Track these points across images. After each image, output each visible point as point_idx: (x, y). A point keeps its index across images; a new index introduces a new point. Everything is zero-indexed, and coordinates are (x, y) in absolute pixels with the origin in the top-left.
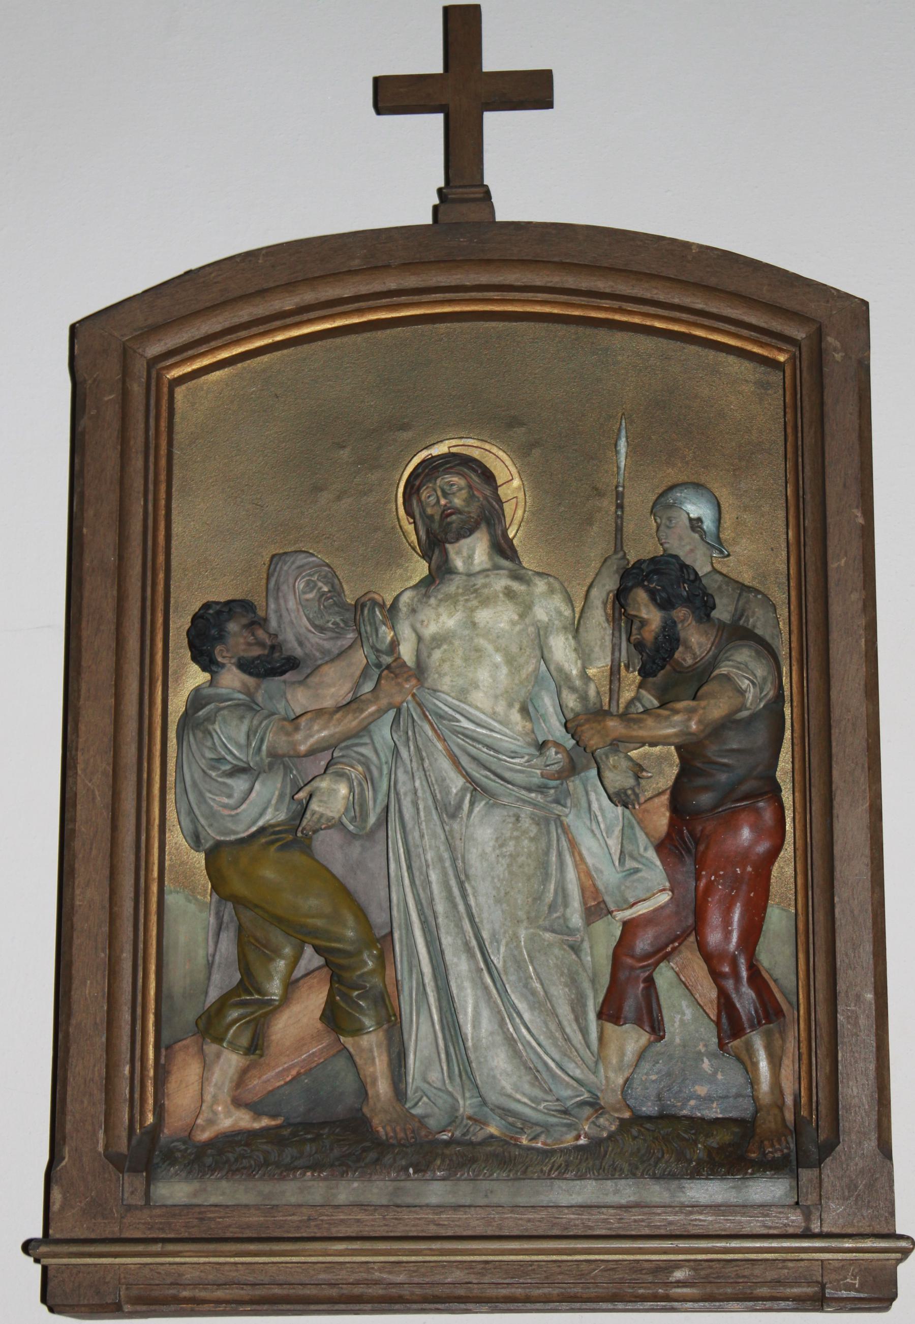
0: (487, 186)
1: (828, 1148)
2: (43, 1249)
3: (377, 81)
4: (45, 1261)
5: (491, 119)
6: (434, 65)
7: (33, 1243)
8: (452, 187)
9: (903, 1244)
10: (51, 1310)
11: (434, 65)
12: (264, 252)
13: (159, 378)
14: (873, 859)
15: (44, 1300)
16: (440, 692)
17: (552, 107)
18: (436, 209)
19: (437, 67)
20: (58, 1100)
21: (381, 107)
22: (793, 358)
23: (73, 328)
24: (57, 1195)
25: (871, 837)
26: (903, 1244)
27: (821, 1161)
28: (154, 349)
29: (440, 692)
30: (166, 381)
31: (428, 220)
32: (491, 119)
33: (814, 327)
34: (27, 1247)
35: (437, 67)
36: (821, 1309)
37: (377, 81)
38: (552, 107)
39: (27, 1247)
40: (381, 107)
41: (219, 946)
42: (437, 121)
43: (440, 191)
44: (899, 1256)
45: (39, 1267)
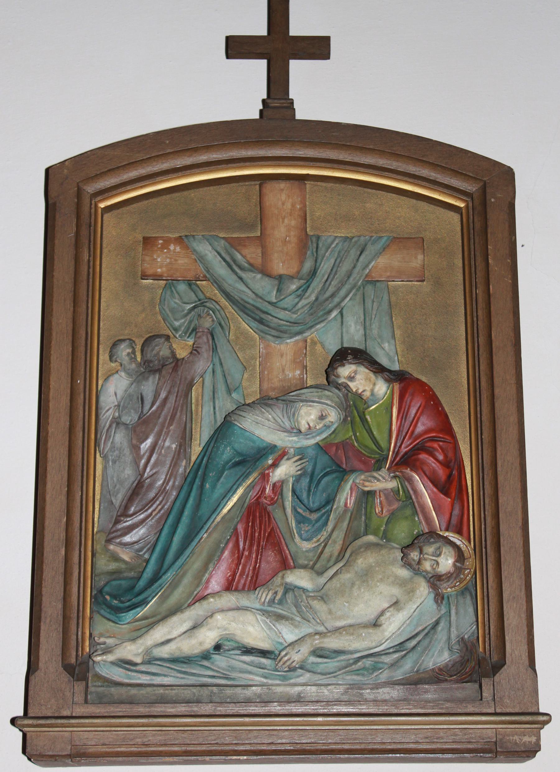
0: (292, 102)
1: (497, 667)
2: (26, 722)
3: (228, 38)
4: (25, 729)
9: (541, 718)
10: (29, 759)
12: (469, 154)
13: (96, 206)
15: (24, 752)
18: (261, 111)
19: (264, 32)
21: (326, 41)
22: (467, 207)
23: (47, 171)
25: (518, 411)
26: (541, 718)
27: (494, 675)
28: (91, 188)
30: (100, 211)
31: (257, 116)
33: (482, 184)
34: (13, 721)
35: (264, 32)
36: (493, 760)
37: (228, 38)
39: (13, 721)
40: (326, 41)
41: (366, 304)
43: (264, 101)
44: (539, 726)
45: (21, 734)
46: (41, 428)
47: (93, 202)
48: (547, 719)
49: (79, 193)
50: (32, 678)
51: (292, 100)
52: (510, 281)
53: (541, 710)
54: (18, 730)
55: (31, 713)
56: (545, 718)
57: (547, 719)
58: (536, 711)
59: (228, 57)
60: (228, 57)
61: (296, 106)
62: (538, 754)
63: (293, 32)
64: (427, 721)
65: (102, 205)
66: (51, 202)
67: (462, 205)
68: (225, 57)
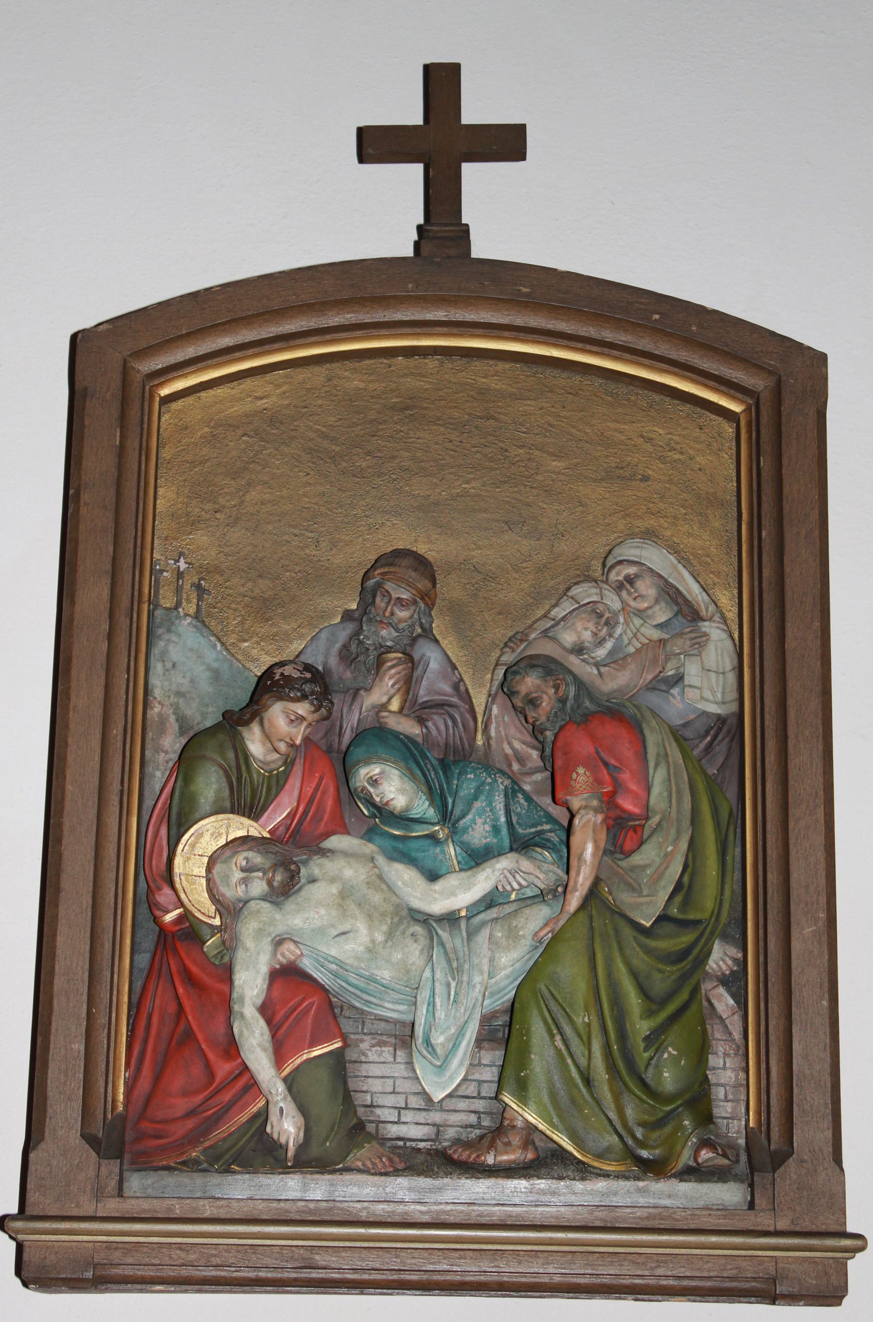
0: (466, 230)
1: (779, 1159)
2: (19, 1225)
3: (360, 131)
4: (20, 1237)
5: (469, 170)
6: (414, 116)
7: (80, 336)
8: (433, 225)
10: (25, 1284)
11: (414, 116)
14: (824, 773)
15: (18, 1272)
16: (379, 1106)
17: (524, 158)
20: (38, 1047)
21: (519, 131)
22: (748, 410)
23: (74, 338)
24: (105, 326)
29: (379, 1106)
31: (409, 252)
32: (469, 170)
38: (524, 158)
40: (519, 131)
42: (417, 170)
43: (420, 228)
45: (13, 1245)
46: (57, 737)
47: (147, 388)
48: (859, 1242)
49: (126, 371)
50: (32, 1156)
51: (467, 225)
52: (533, 1056)
53: (850, 1228)
54: (7, 1236)
55: (29, 1211)
56: (859, 1243)
57: (859, 1242)
58: (834, 1228)
59: (361, 159)
60: (361, 159)
61: (472, 237)
62: (845, 1301)
63: (464, 121)
64: (630, 1241)
65: (165, 391)
66: (78, 386)
67: (736, 407)
68: (356, 161)
